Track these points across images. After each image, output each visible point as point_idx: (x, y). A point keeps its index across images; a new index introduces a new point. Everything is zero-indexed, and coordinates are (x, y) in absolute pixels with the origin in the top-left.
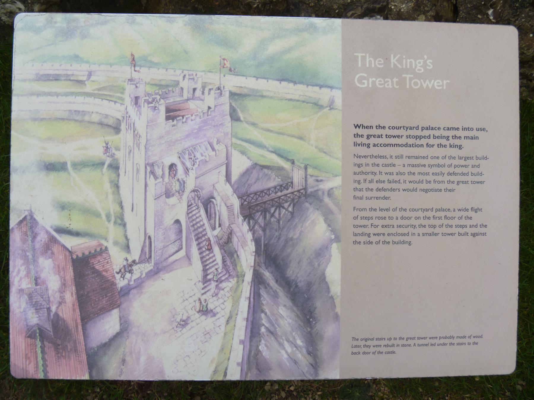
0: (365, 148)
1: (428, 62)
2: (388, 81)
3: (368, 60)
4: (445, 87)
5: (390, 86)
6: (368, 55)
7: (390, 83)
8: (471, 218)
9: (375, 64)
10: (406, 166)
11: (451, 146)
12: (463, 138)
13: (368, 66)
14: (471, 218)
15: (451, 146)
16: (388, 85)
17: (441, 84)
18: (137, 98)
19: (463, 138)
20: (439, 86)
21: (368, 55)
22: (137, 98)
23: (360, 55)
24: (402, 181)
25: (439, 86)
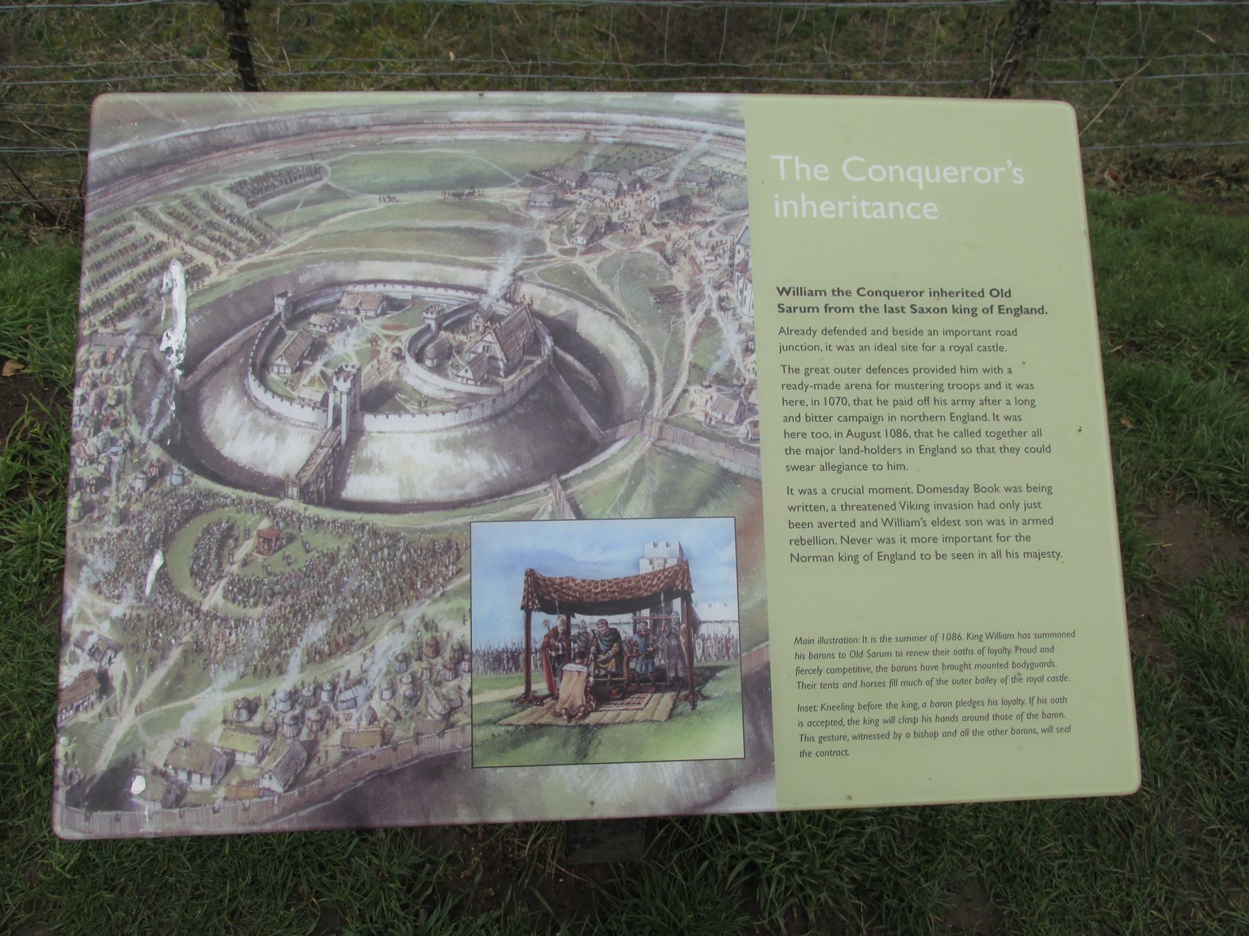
0: (968, 316)
1: (1014, 172)
2: (878, 207)
3: (798, 167)
4: (841, 215)
5: (883, 216)
6: (797, 158)
7: (882, 210)
8: (1028, 538)
9: (812, 173)
10: (908, 540)
11: (955, 311)
12: (803, 452)
13: (798, 178)
14: (1028, 538)
15: (955, 311)
16: (879, 214)
17: (956, 173)
18: (257, 890)
19: (803, 452)
20: (953, 177)
21: (797, 158)
22: (257, 890)
23: (782, 158)
24: (990, 417)
25: (828, 212)
